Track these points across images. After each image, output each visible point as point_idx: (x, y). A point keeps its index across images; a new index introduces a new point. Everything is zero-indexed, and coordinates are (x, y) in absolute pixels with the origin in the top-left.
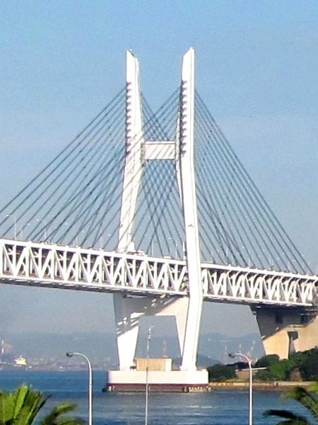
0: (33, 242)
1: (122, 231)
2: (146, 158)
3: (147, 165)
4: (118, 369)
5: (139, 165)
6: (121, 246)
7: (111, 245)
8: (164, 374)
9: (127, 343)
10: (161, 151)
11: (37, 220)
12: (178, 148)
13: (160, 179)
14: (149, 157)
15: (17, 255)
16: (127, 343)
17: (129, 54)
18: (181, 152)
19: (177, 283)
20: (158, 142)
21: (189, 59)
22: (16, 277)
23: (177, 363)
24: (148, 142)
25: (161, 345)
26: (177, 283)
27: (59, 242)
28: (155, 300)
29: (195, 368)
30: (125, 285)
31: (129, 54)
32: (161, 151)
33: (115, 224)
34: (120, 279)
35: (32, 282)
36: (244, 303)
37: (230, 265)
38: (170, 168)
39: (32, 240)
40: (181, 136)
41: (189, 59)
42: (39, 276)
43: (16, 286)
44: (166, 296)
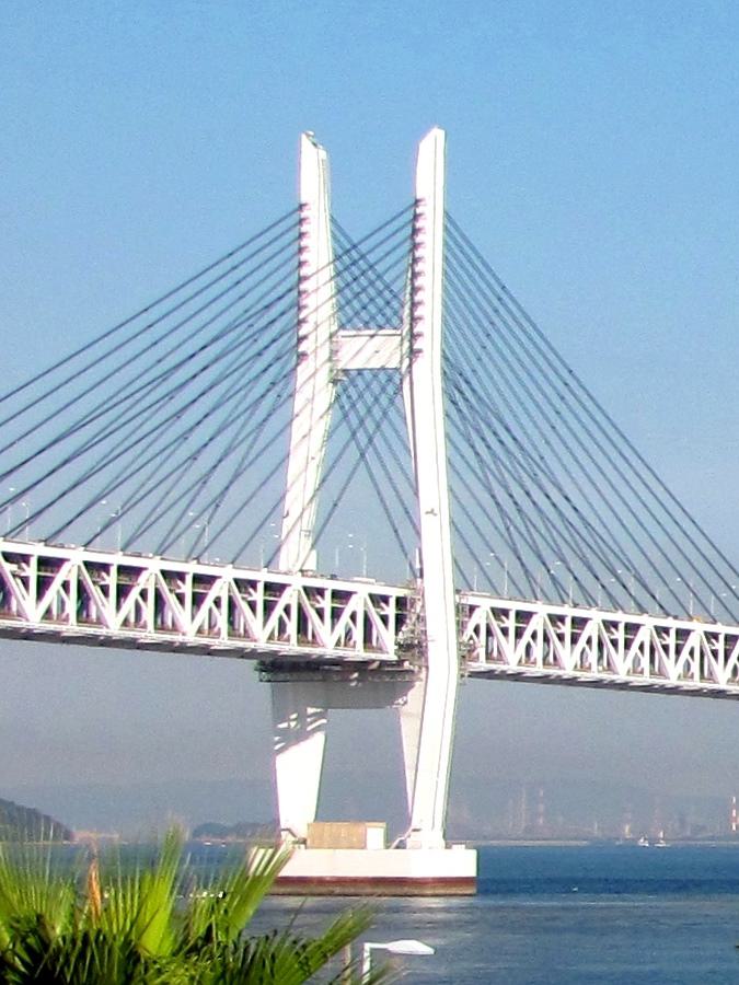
0: (199, 563)
1: (309, 521)
2: (341, 366)
3: (346, 381)
4: (364, 847)
5: (323, 376)
6: (286, 560)
7: (261, 550)
8: (369, 857)
9: (298, 774)
10: (374, 351)
11: (191, 514)
12: (406, 344)
13: (368, 403)
14: (346, 365)
15: (677, 645)
16: (298, 774)
17: (306, 143)
18: (413, 353)
19: (387, 638)
20: (354, 333)
21: (431, 151)
22: (37, 626)
23: (398, 827)
24: (342, 333)
25: (366, 792)
26: (387, 638)
27: (161, 552)
28: (356, 675)
29: (443, 842)
30: (599, 672)
31: (306, 143)
32: (374, 351)
33: (261, 506)
34: (692, 670)
35: (492, 671)
36: (240, 653)
37: (620, 612)
38: (391, 383)
39: (197, 559)
40: (414, 320)
41: (431, 151)
42: (670, 676)
43: (241, 660)
44: (380, 666)
